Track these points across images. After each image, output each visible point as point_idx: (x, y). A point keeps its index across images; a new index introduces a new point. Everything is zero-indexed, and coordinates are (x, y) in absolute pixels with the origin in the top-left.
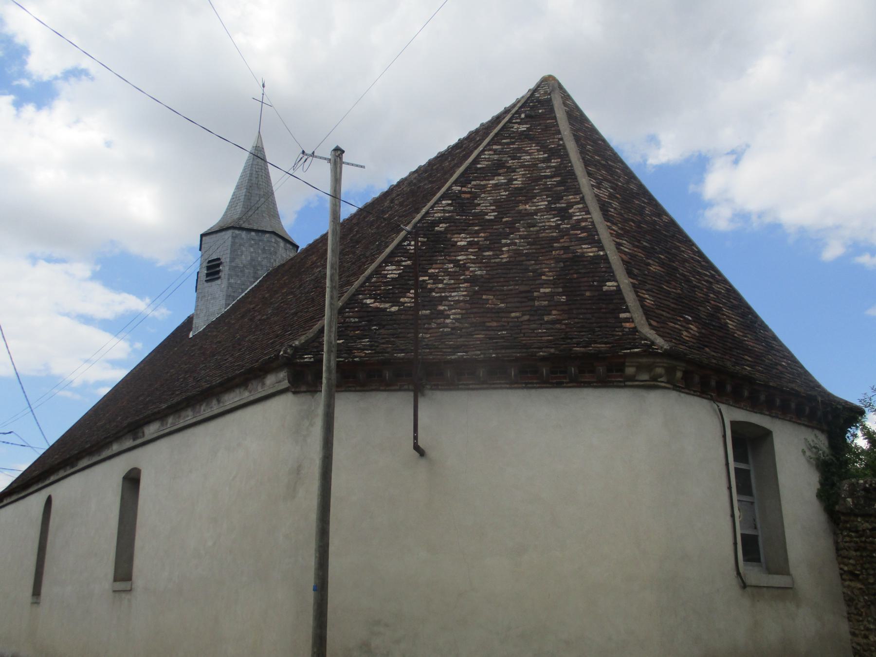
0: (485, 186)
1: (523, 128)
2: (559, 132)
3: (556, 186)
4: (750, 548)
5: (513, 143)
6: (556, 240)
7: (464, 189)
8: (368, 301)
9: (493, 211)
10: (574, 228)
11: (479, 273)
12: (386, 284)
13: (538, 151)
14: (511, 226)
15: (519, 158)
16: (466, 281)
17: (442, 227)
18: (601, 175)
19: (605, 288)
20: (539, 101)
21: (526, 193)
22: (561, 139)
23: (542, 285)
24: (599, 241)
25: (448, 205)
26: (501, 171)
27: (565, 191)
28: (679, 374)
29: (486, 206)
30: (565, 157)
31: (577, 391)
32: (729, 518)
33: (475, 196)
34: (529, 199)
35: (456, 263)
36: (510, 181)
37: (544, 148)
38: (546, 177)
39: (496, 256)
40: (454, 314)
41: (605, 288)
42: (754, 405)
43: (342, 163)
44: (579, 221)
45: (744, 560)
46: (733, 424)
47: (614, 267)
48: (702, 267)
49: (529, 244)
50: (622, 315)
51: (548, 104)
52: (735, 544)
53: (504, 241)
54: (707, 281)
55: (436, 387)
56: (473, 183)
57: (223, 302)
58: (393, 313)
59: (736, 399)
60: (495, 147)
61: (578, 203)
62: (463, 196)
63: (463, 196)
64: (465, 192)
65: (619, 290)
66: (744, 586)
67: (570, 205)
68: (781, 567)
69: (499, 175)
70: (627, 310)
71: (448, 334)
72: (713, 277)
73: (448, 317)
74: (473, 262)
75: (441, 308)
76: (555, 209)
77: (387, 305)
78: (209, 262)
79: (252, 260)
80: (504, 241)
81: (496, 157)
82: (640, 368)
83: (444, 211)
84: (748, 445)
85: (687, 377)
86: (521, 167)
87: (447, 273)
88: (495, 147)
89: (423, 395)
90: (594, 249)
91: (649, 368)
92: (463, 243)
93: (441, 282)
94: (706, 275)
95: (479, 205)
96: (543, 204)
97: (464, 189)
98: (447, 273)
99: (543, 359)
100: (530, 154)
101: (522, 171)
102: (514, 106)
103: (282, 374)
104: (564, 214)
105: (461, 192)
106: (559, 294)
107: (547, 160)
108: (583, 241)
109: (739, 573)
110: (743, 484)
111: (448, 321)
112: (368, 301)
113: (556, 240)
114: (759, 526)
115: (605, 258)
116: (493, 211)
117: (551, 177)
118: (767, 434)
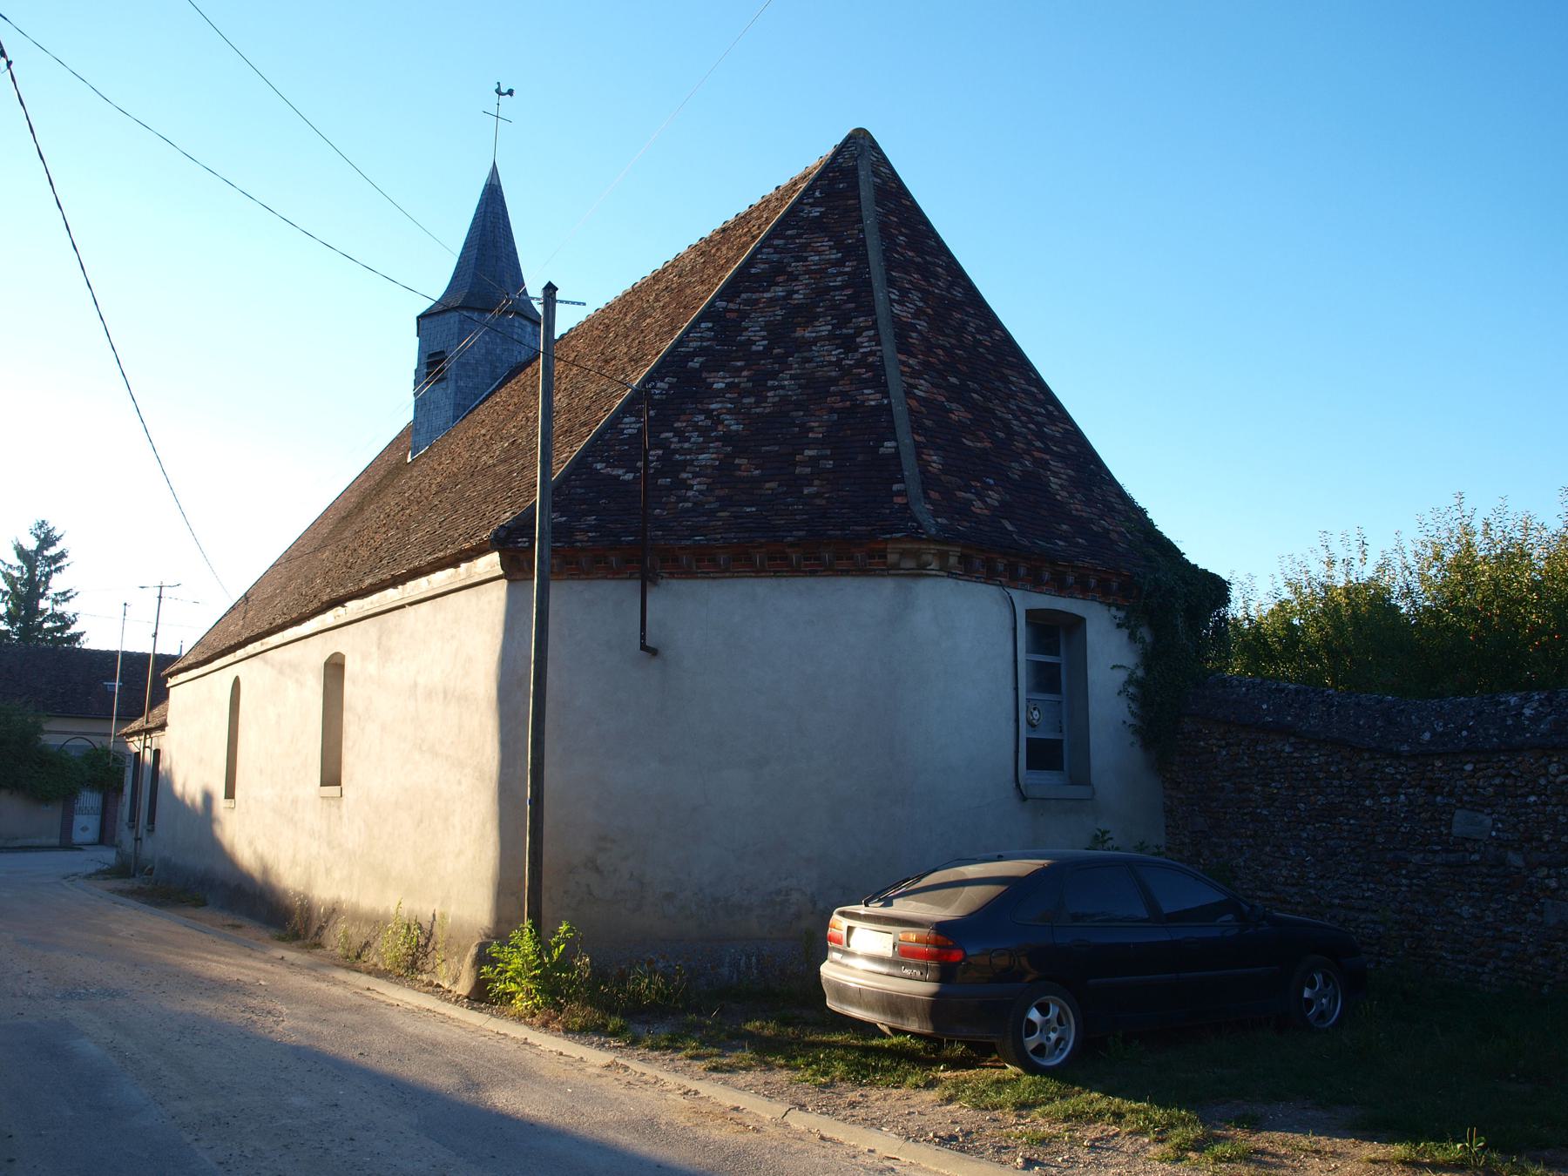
0: (757, 301)
1: (816, 212)
2: (860, 221)
3: (846, 302)
4: (1042, 754)
5: (799, 236)
6: (834, 381)
7: (731, 306)
8: (599, 466)
9: (764, 338)
10: (858, 364)
11: (734, 428)
12: (622, 442)
13: (831, 248)
14: (781, 360)
15: (805, 259)
16: (717, 439)
17: (696, 363)
18: (910, 282)
19: (882, 450)
20: (841, 170)
21: (807, 314)
22: (862, 231)
23: (808, 446)
24: (885, 385)
25: (709, 329)
26: (781, 279)
27: (855, 309)
28: (953, 560)
29: (755, 334)
30: (863, 259)
31: (833, 580)
32: (1012, 723)
33: (744, 316)
34: (811, 319)
35: (709, 414)
36: (790, 294)
37: (839, 245)
38: (836, 288)
39: (757, 404)
40: (698, 485)
41: (882, 450)
42: (1061, 589)
43: (555, 301)
44: (866, 355)
45: (1028, 768)
46: (1030, 614)
47: (897, 422)
48: (1037, 402)
49: (800, 386)
50: (895, 487)
51: (851, 174)
52: (1017, 752)
53: (770, 383)
54: (1036, 423)
55: (672, 576)
56: (744, 296)
57: (451, 413)
58: (627, 482)
59: (1036, 583)
60: (776, 242)
61: (868, 328)
62: (729, 315)
63: (729, 315)
64: (731, 311)
65: (897, 454)
66: (1024, 799)
67: (859, 331)
68: (1081, 777)
69: (777, 284)
70: (902, 481)
71: (687, 510)
72: (1049, 415)
73: (690, 487)
74: (729, 412)
75: (684, 475)
76: (837, 337)
77: (620, 472)
78: (430, 356)
79: (488, 352)
80: (770, 383)
81: (776, 257)
82: (904, 554)
83: (702, 339)
84: (1052, 637)
85: (965, 560)
86: (806, 273)
87: (696, 428)
88: (776, 242)
89: (655, 584)
90: (878, 396)
91: (916, 555)
92: (721, 385)
93: (688, 440)
94: (1038, 414)
95: (746, 329)
96: (825, 330)
97: (731, 306)
98: (696, 428)
99: (791, 545)
100: (819, 253)
101: (805, 279)
102: (803, 178)
103: (495, 557)
104: (849, 344)
105: (726, 310)
106: (826, 458)
107: (839, 263)
108: (866, 383)
109: (1018, 785)
110: (1046, 679)
111: (690, 493)
112: (599, 466)
113: (834, 381)
114: (1065, 728)
115: (888, 409)
116: (764, 338)
117: (841, 288)
118: (1078, 623)
